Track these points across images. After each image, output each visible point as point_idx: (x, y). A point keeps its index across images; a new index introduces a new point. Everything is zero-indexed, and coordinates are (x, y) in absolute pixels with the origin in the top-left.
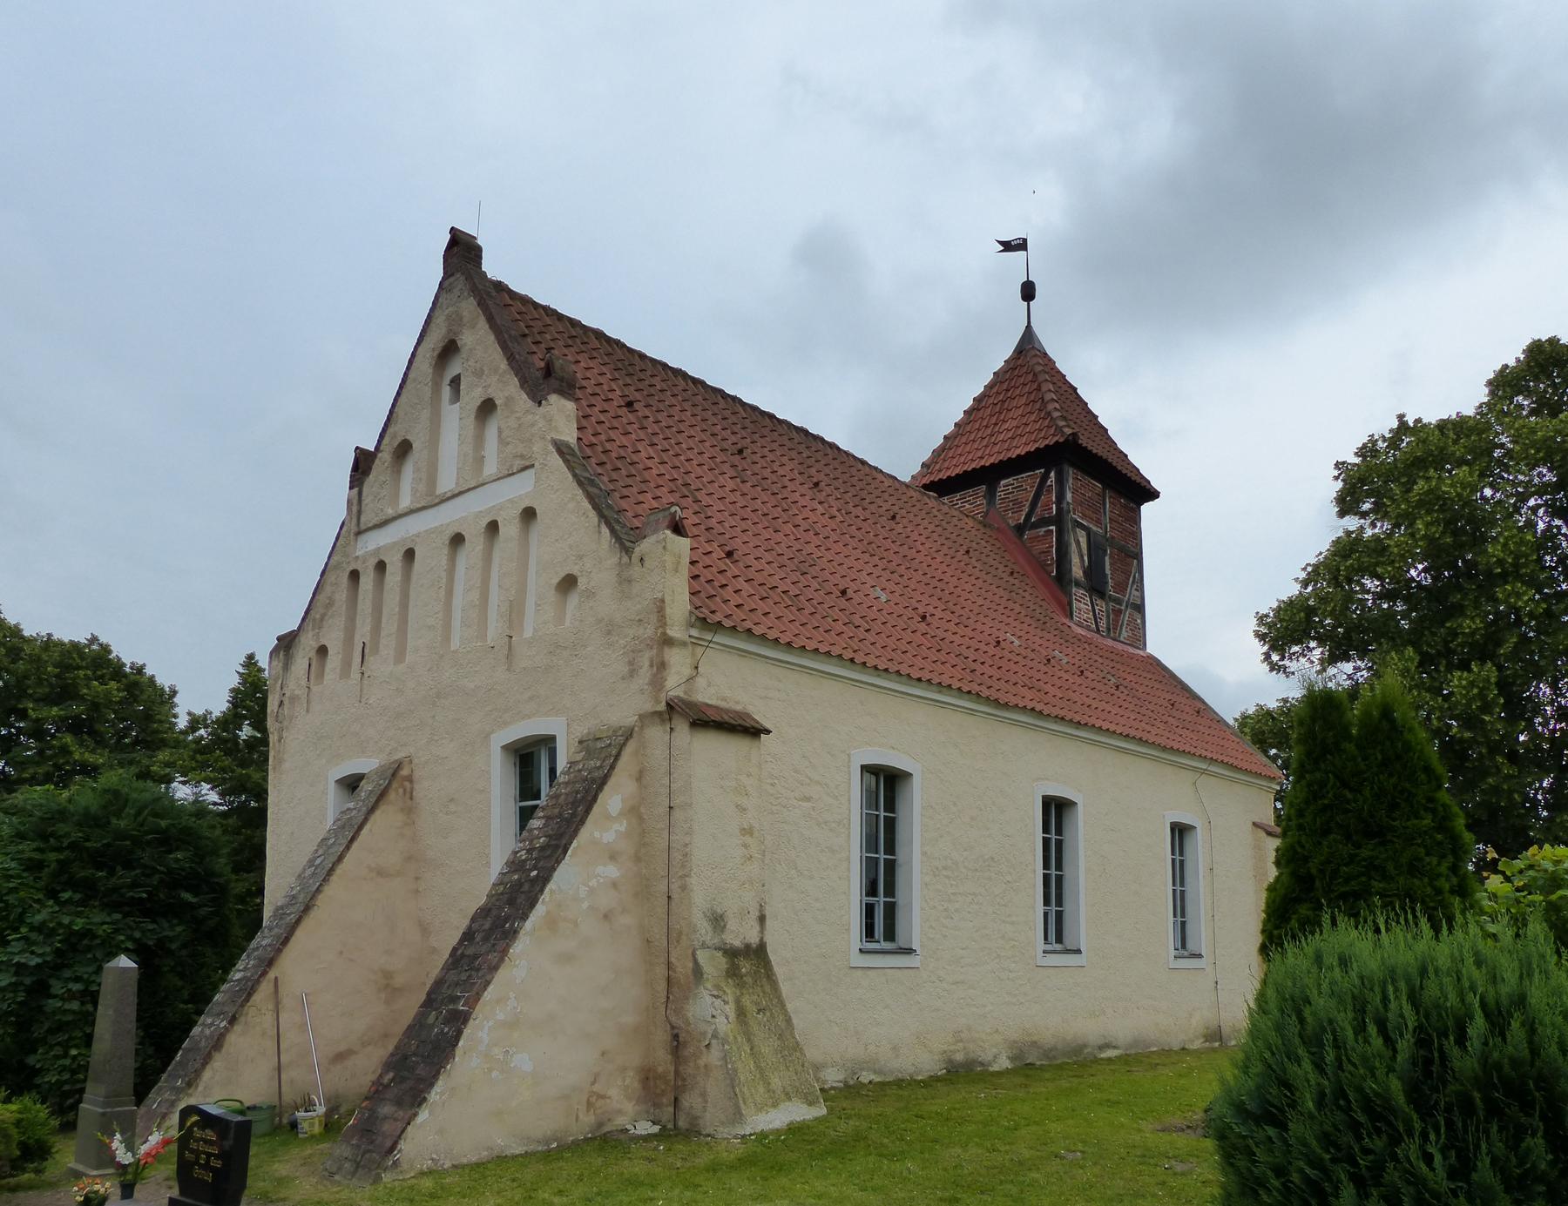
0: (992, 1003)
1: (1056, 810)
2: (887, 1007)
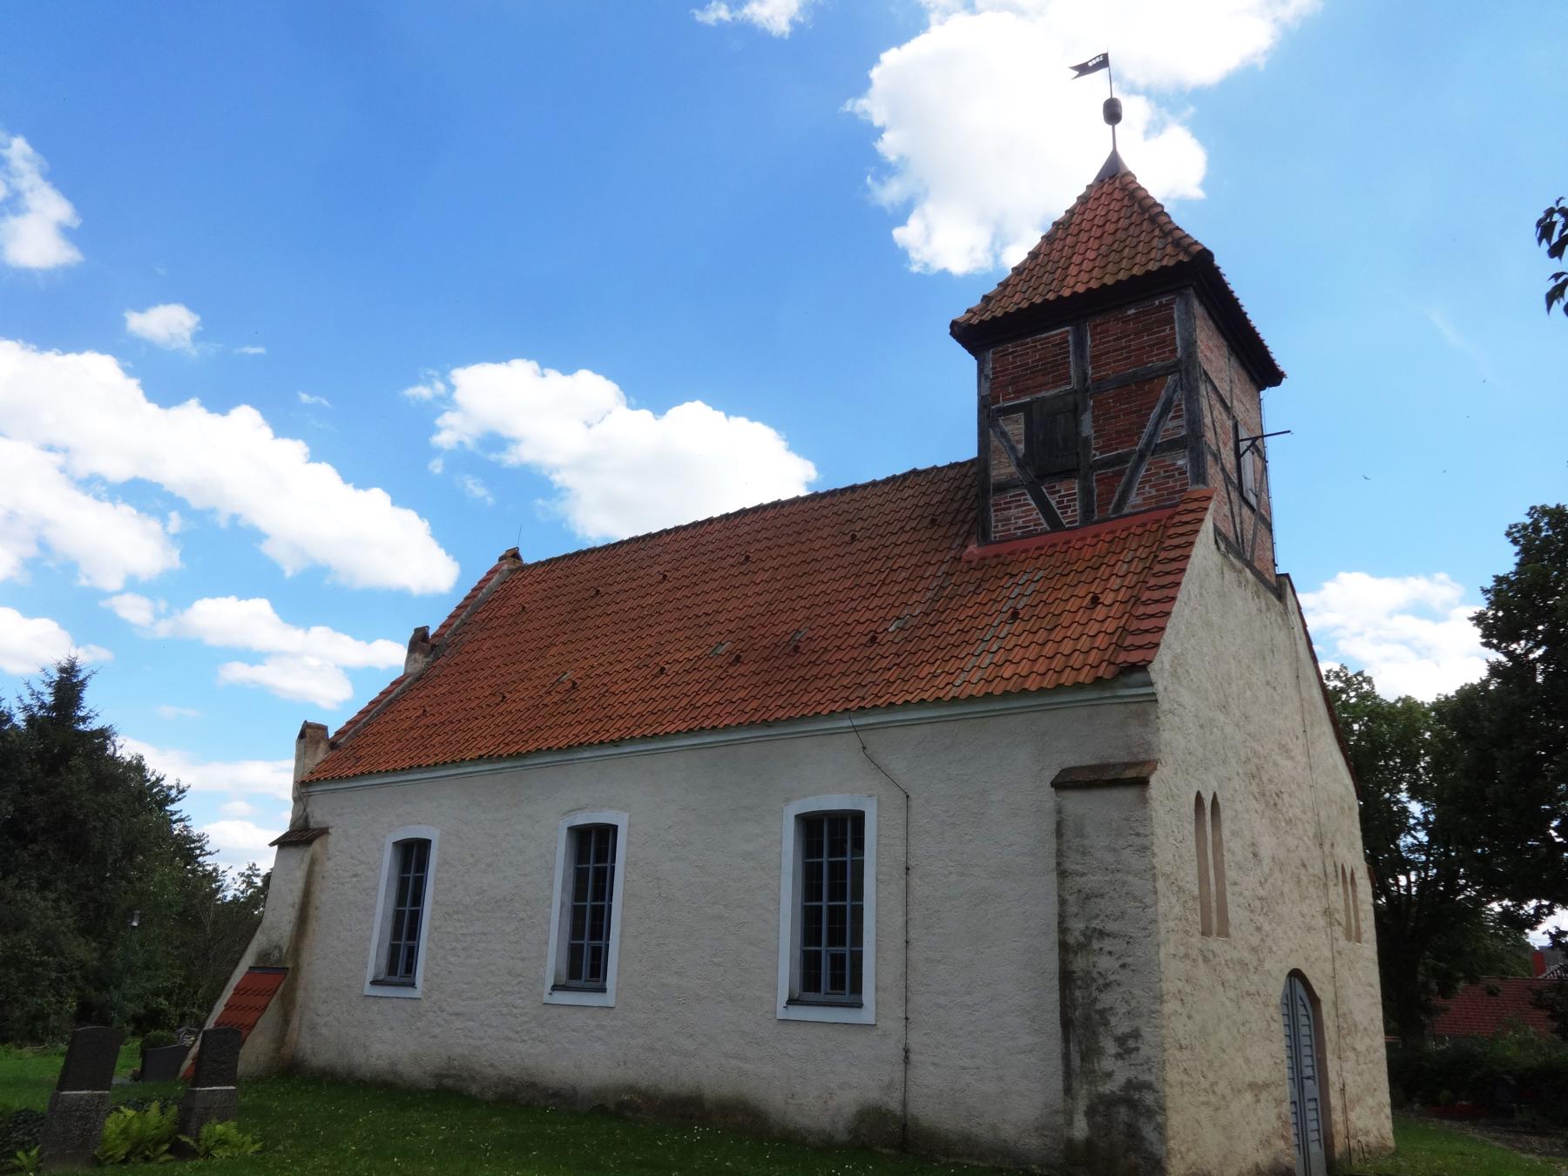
0: (489, 1037)
1: (413, 855)
2: (392, 1029)
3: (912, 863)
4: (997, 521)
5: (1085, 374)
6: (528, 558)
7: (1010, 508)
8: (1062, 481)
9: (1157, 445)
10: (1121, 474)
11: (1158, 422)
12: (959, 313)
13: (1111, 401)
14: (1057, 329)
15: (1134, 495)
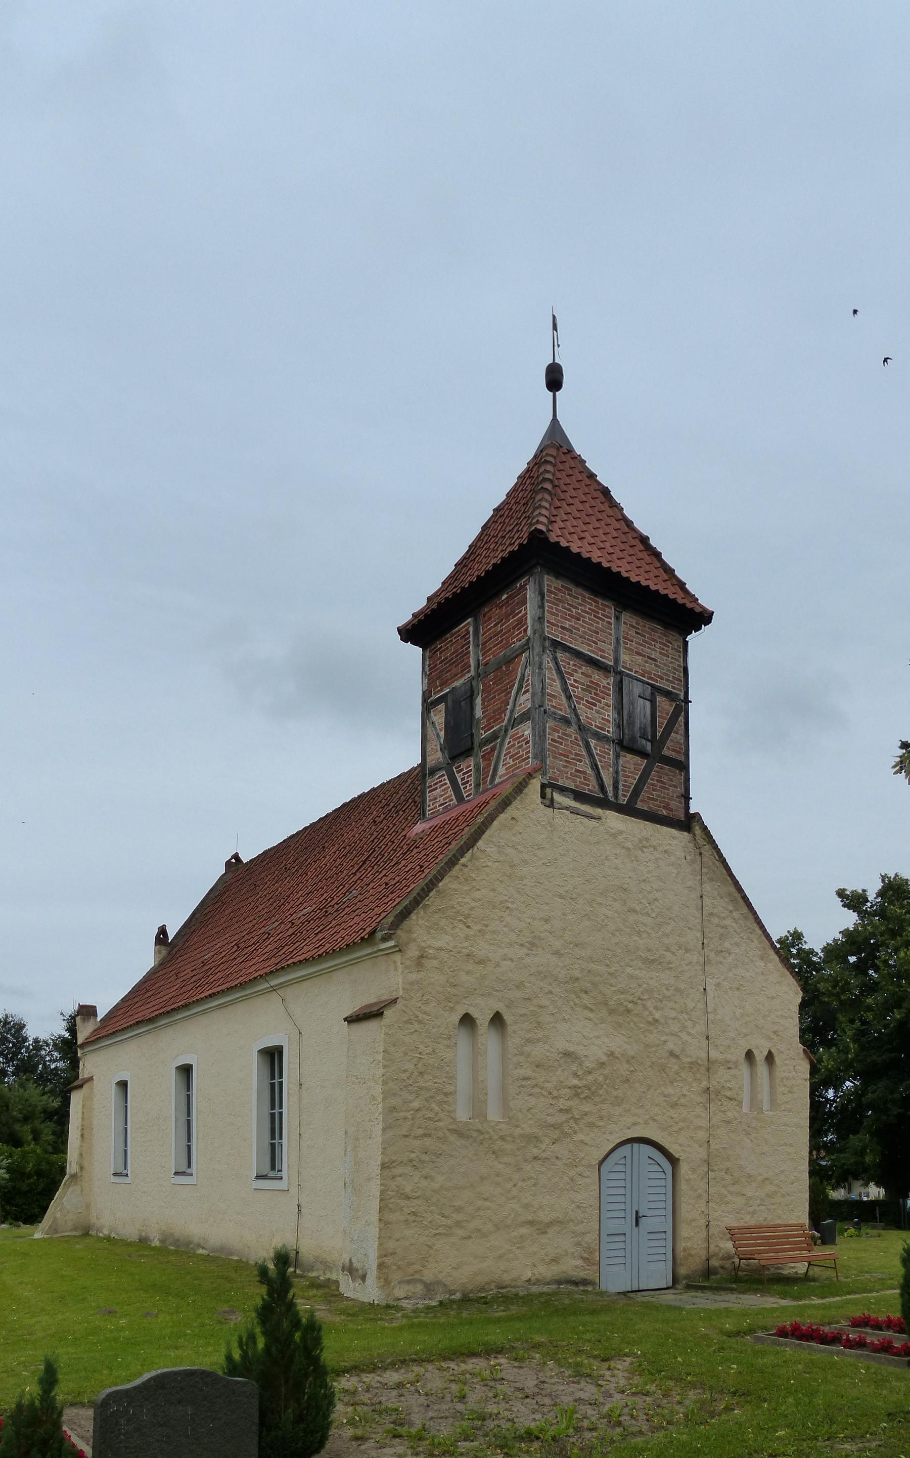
3: (302, 1081)
4: (430, 801)
5: (478, 660)
6: (245, 860)
7: (436, 789)
8: (464, 760)
9: (515, 719)
10: (493, 749)
11: (515, 700)
12: (405, 617)
13: (491, 683)
14: (463, 622)
15: (501, 766)
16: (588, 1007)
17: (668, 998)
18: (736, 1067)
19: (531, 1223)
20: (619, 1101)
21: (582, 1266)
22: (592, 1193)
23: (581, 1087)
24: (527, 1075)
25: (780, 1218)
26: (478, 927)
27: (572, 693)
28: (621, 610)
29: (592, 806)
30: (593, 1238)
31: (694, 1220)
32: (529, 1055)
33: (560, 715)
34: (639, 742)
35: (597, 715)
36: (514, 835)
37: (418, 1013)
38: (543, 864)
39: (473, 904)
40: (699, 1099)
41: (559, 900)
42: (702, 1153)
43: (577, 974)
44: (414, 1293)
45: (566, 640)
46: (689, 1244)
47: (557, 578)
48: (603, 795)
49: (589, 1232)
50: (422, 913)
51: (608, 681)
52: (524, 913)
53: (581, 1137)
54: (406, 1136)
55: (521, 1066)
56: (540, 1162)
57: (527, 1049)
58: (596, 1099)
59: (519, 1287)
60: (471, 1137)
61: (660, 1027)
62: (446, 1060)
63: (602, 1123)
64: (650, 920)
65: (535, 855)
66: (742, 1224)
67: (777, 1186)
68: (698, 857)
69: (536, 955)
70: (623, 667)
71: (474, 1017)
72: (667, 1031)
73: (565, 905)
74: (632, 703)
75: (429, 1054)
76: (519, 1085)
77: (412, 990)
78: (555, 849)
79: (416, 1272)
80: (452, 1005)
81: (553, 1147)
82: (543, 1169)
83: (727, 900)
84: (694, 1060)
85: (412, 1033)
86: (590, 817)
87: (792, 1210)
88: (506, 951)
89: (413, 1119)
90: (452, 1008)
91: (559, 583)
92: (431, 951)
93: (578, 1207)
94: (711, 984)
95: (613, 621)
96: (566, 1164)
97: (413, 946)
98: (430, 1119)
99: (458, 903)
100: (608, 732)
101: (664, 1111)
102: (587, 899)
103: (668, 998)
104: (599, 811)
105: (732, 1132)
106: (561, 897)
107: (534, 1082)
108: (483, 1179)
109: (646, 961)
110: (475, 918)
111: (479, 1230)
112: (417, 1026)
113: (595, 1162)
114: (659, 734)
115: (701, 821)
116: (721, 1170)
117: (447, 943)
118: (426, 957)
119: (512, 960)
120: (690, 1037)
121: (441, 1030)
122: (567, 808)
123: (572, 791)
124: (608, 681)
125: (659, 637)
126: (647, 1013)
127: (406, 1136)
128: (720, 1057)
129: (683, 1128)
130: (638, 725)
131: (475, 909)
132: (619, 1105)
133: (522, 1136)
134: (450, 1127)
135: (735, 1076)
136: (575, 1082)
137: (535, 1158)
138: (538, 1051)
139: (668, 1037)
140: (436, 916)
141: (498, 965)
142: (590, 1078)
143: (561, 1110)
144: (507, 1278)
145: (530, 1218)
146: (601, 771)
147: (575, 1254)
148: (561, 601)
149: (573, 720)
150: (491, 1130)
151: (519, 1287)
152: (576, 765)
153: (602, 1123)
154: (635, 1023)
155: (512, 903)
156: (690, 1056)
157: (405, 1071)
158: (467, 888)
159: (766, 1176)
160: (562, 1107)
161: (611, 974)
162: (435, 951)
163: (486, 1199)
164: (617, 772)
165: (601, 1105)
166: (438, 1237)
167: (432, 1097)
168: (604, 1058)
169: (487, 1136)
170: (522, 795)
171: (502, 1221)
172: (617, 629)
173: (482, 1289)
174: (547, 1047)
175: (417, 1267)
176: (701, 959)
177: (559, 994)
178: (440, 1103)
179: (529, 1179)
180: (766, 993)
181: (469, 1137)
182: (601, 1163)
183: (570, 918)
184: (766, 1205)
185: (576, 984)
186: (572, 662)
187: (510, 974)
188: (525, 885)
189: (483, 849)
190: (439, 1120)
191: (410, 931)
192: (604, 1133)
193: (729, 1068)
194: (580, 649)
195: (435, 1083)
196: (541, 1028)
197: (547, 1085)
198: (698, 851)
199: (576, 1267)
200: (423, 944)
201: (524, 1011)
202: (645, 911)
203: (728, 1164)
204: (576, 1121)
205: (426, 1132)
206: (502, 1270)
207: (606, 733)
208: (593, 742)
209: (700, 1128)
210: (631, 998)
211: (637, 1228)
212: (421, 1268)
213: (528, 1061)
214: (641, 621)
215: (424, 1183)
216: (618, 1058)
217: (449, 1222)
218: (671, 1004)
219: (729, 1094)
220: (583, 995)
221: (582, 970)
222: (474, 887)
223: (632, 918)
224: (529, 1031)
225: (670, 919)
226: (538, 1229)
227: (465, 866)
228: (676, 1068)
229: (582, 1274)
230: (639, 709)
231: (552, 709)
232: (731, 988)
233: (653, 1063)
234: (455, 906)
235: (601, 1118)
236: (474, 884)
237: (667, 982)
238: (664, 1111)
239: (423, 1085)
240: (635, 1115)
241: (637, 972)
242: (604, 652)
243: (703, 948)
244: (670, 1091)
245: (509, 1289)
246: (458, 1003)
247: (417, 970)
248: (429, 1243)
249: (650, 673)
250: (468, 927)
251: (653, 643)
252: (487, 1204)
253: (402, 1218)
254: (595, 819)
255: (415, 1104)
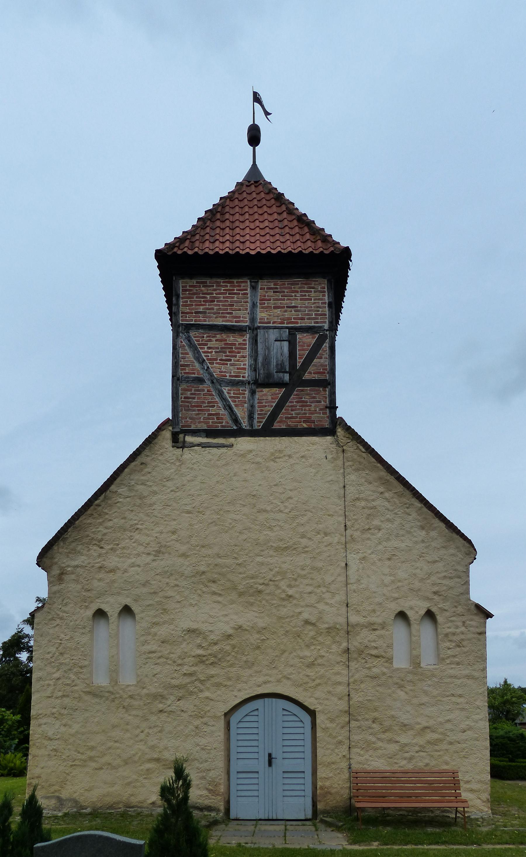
16: (217, 593)
17: (304, 577)
18: (383, 628)
19: (158, 760)
20: (250, 665)
21: (207, 796)
22: (216, 739)
23: (206, 656)
24: (153, 649)
25: (447, 763)
26: (109, 547)
27: (205, 358)
28: (256, 280)
29: (224, 438)
30: (218, 774)
31: (333, 763)
32: (155, 634)
33: (194, 377)
34: (275, 376)
35: (232, 368)
36: (143, 475)
37: (58, 612)
38: (172, 491)
39: (105, 531)
40: (339, 659)
41: (187, 515)
42: (343, 705)
43: (202, 568)
44: (48, 806)
45: (200, 321)
46: (327, 784)
47: (191, 278)
48: (236, 426)
49: (213, 769)
50: (62, 544)
51: (245, 338)
52: (152, 530)
53: (207, 694)
54: (50, 697)
55: (148, 643)
56: (166, 714)
57: (153, 630)
58: (225, 664)
59: (144, 808)
60: (104, 696)
61: (295, 602)
62: (81, 643)
63: (229, 683)
64: (283, 515)
65: (164, 486)
66: (396, 768)
67: (442, 733)
68: (341, 455)
69: (162, 560)
70: (260, 323)
71: (105, 611)
72: (302, 604)
73: (192, 518)
74: (268, 348)
75: (67, 640)
76: (145, 657)
77: (55, 597)
78: (183, 478)
79: (56, 791)
80: (86, 604)
81: (178, 702)
82: (169, 720)
83: (376, 484)
84: (331, 625)
85: (55, 627)
86: (223, 446)
87: (464, 757)
88: (133, 560)
89: (54, 685)
90: (87, 606)
91: (194, 282)
92: (69, 569)
93: (203, 749)
94: (353, 559)
95: (249, 291)
96: (191, 716)
97: (55, 567)
98: (68, 685)
99: (93, 532)
100: (243, 377)
101: (300, 670)
102: (214, 510)
103: (304, 577)
104: (232, 440)
105: (379, 685)
106: (189, 512)
107: (160, 654)
108: (114, 727)
109: (277, 549)
110: (107, 541)
111: (109, 764)
112: (58, 621)
113: (221, 714)
114: (299, 365)
115: (344, 423)
116: (367, 720)
117: (83, 562)
118: (66, 574)
119: (139, 566)
120: (328, 607)
121: (77, 622)
122: (198, 445)
123: (204, 431)
124: (245, 338)
125: (300, 288)
126: (279, 591)
127: (50, 697)
128: (362, 620)
129: (319, 684)
130: (274, 363)
131: (108, 534)
132: (250, 668)
133: (148, 695)
134: (85, 690)
135: (380, 637)
136: (200, 652)
137: (161, 711)
138: (163, 631)
139: (303, 609)
140: (74, 544)
141: (126, 571)
142: (216, 648)
143: (185, 674)
144: (134, 800)
145: (156, 756)
146: (235, 409)
147: (200, 786)
148: (194, 294)
149: (206, 377)
150: (121, 692)
151: (144, 808)
152: (209, 410)
153: (229, 683)
154: (267, 601)
155: (142, 524)
156: (327, 623)
157: (49, 653)
158: (101, 520)
159: (426, 724)
160: (185, 672)
161: (239, 564)
162: (72, 569)
163: (116, 742)
164: (252, 406)
165: (228, 669)
166: (75, 767)
167: (70, 670)
168: (231, 631)
169: (117, 696)
170: (152, 445)
171: (130, 758)
172: (254, 295)
173: (111, 807)
174: (172, 627)
175: (56, 788)
176: (343, 539)
177: (186, 586)
178: (76, 674)
179: (154, 727)
180: (427, 558)
181: (101, 697)
182: (228, 714)
183: (196, 527)
184: (427, 752)
185: (204, 577)
186: (205, 336)
187: (137, 577)
188: (154, 509)
189: (114, 491)
190: (75, 685)
191: (52, 558)
192: (233, 691)
193: (375, 630)
194: (214, 323)
195: (72, 660)
196: (167, 613)
197: (172, 655)
198: (341, 449)
199: (201, 796)
200: (63, 565)
201: (151, 602)
202: (277, 509)
203: (376, 714)
204: (202, 682)
205: (65, 693)
206: (129, 794)
207: (241, 378)
208: (225, 390)
209: (339, 683)
210: (261, 581)
211: (270, 768)
212: (60, 789)
213: (154, 639)
214: (279, 282)
215: (63, 729)
216: (247, 630)
217: (83, 757)
218: (306, 581)
219: (374, 652)
220: (210, 584)
221: (209, 565)
222: (106, 519)
223: (261, 517)
224: (155, 616)
225: (306, 511)
226: (164, 765)
227: (99, 505)
228: (312, 633)
229: (207, 802)
230: (275, 351)
231: (185, 375)
232: (380, 560)
233: (287, 632)
234: (90, 535)
235: (229, 679)
236: (107, 516)
237: (301, 564)
238: (300, 670)
239: (63, 661)
240: (266, 675)
241: (269, 559)
242: (240, 317)
243: (346, 530)
244: (307, 653)
245: (136, 809)
246: (92, 602)
247: (59, 583)
248: (67, 772)
249: (290, 319)
250: (102, 548)
251: (293, 294)
252: (117, 745)
253: (47, 753)
254: (226, 446)
255: (57, 675)
